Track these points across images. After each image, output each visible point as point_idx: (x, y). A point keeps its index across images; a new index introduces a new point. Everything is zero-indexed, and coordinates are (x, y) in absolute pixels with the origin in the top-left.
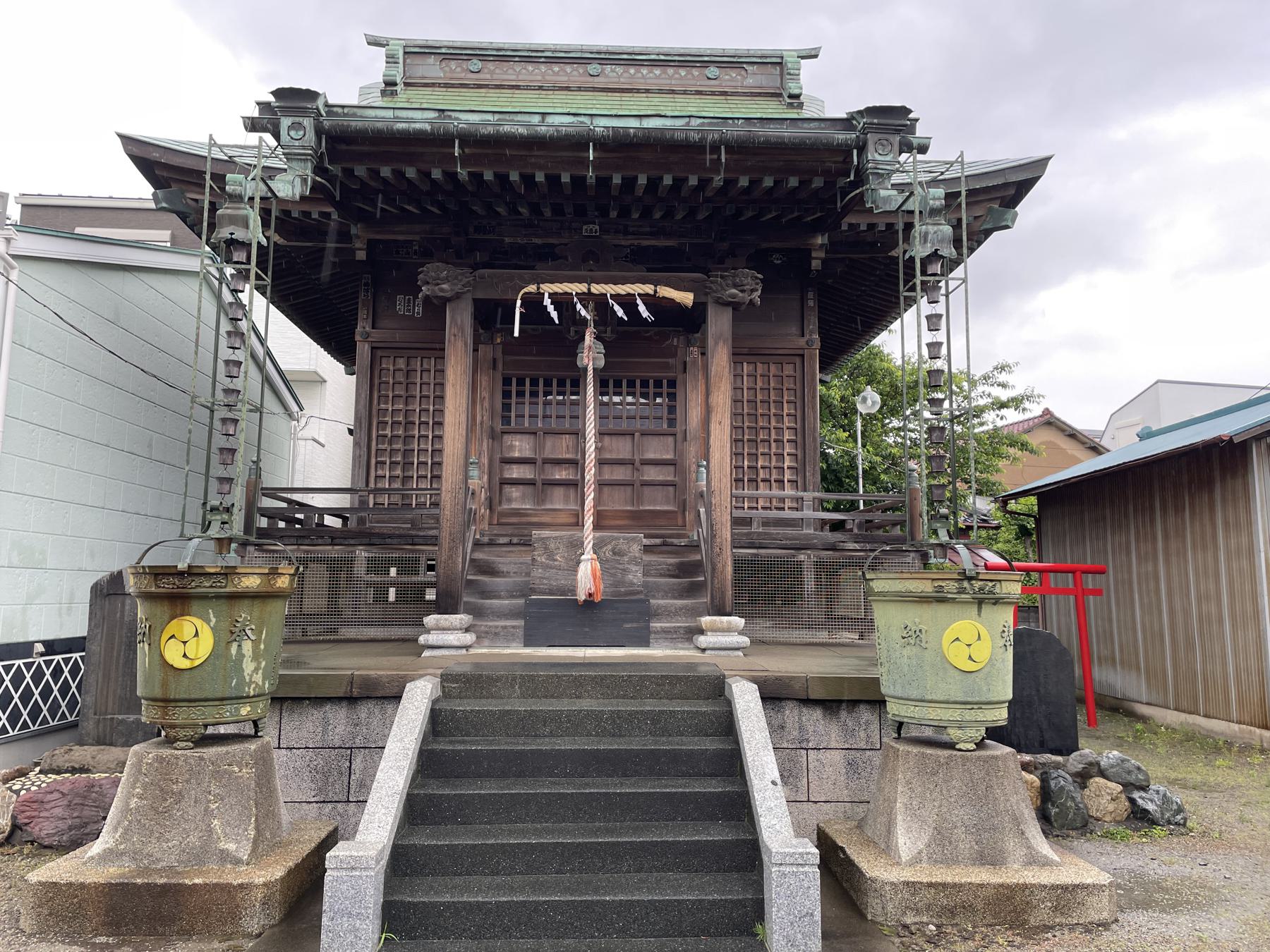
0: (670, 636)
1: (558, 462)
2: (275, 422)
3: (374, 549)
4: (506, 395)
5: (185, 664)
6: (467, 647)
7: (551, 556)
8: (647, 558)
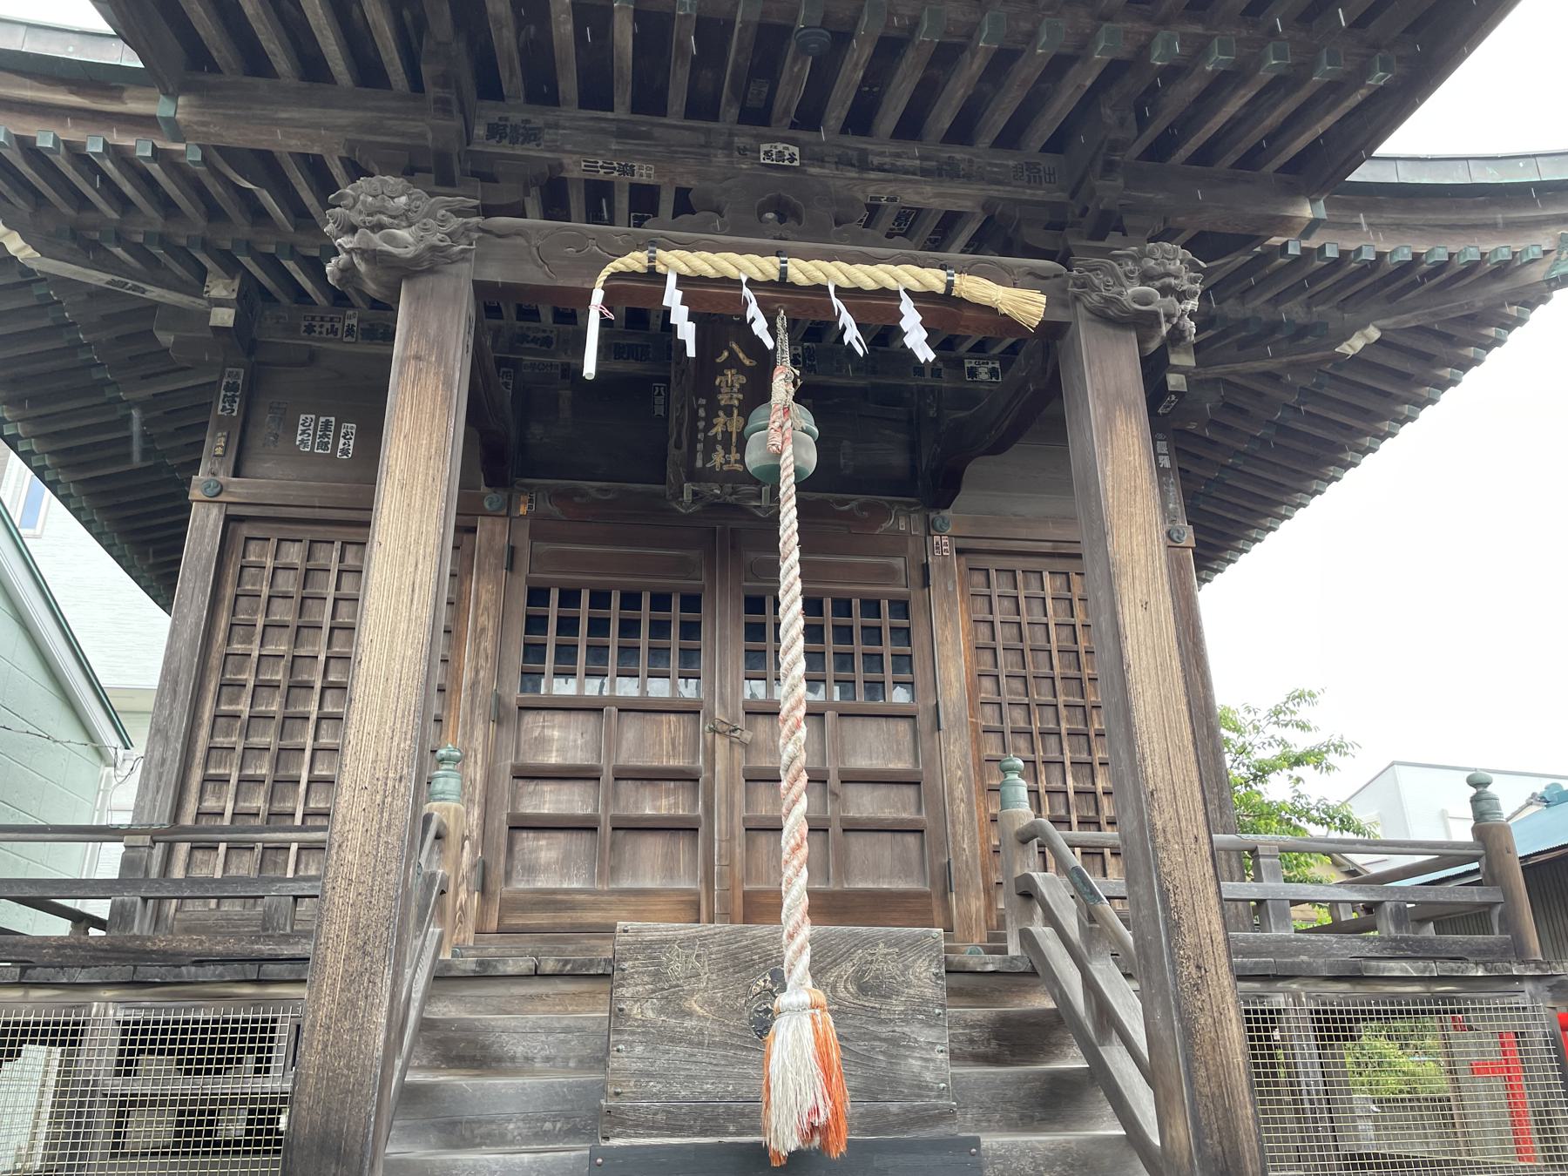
3: (145, 997)
4: (535, 624)
7: (673, 1002)
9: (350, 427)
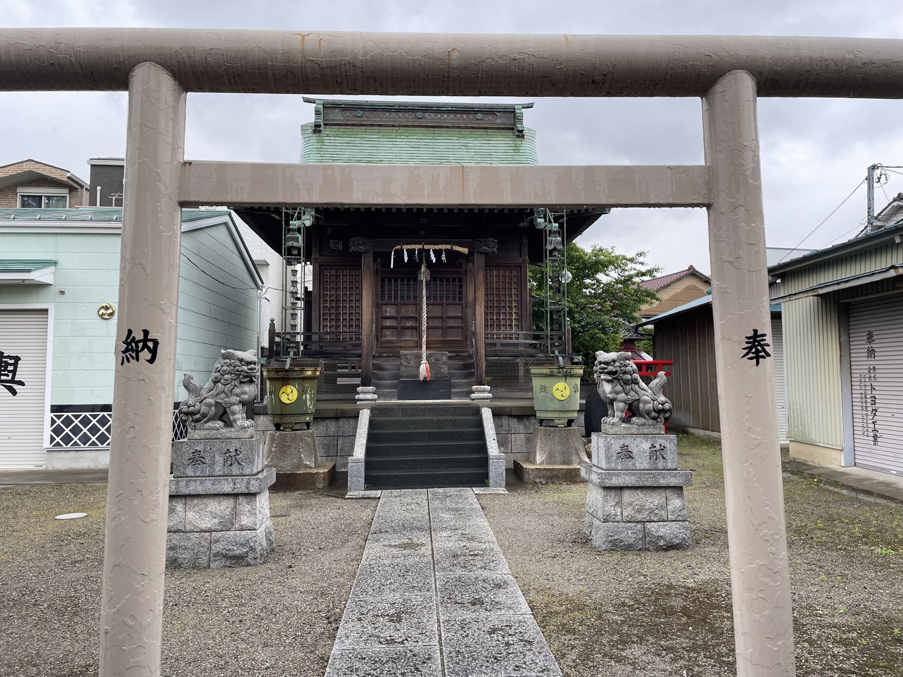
0: (460, 395)
1: (408, 318)
2: (254, 293)
5: (289, 402)
6: (375, 400)
7: (409, 362)
8: (449, 362)
9: (341, 242)
